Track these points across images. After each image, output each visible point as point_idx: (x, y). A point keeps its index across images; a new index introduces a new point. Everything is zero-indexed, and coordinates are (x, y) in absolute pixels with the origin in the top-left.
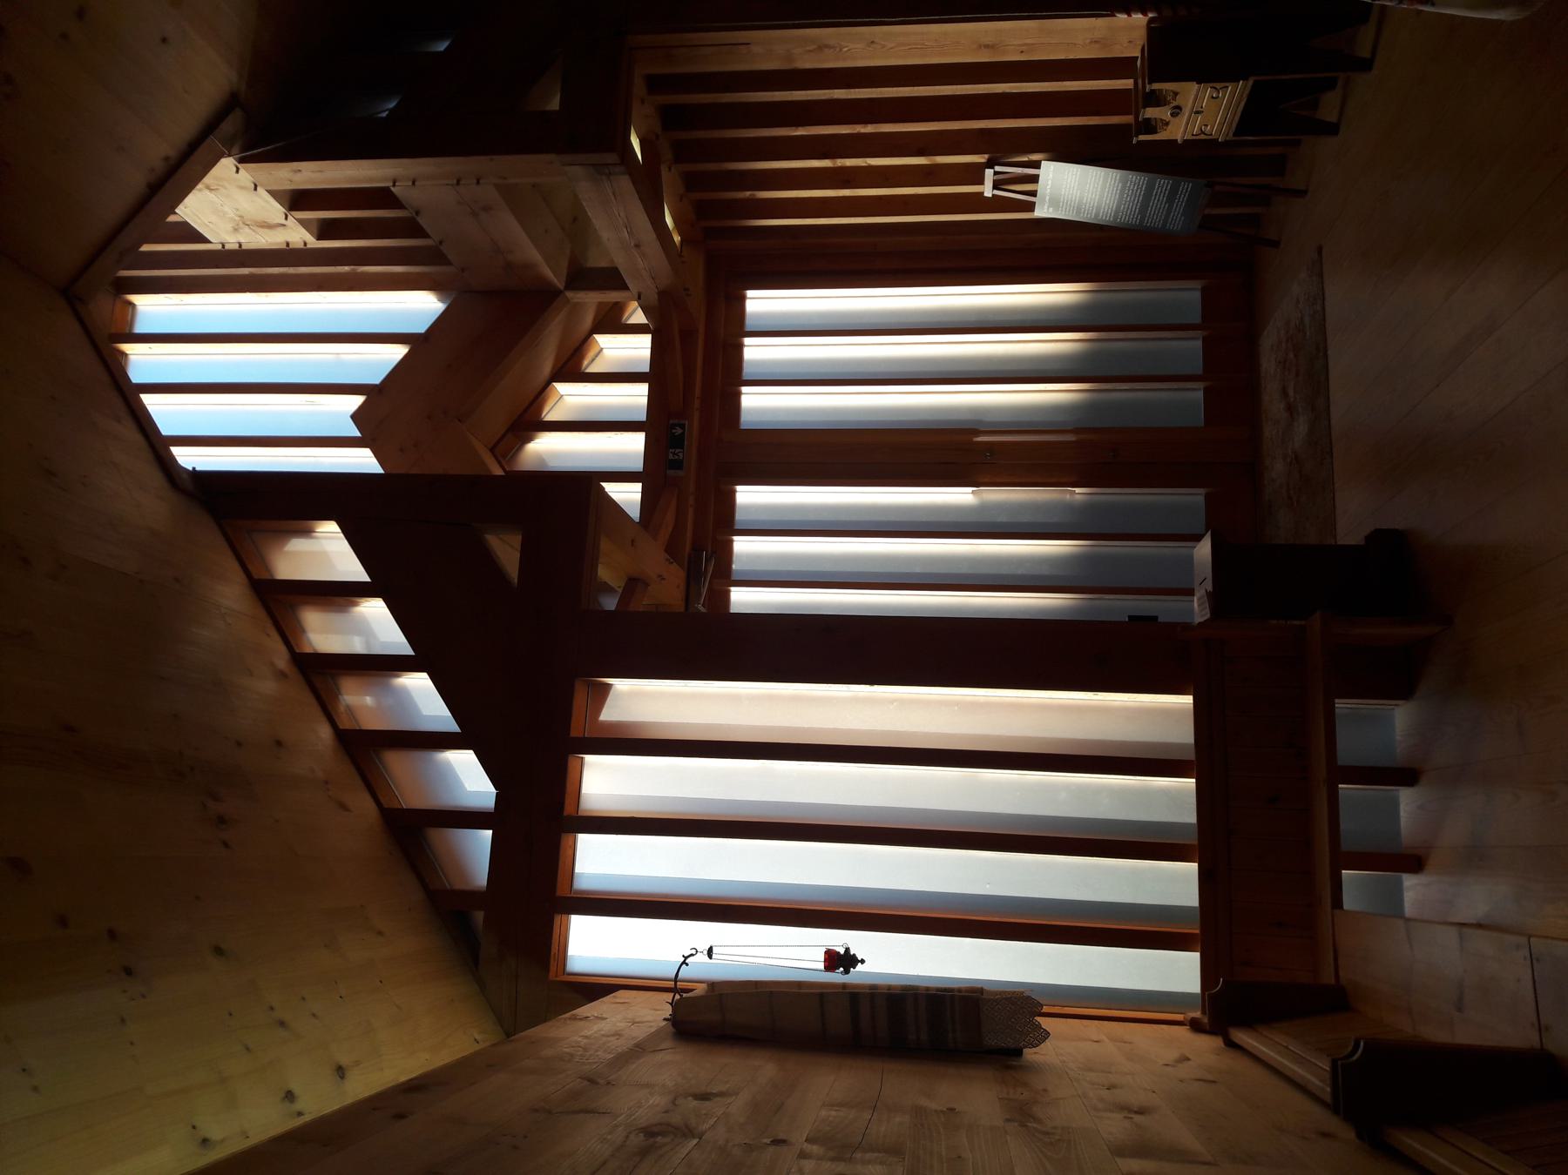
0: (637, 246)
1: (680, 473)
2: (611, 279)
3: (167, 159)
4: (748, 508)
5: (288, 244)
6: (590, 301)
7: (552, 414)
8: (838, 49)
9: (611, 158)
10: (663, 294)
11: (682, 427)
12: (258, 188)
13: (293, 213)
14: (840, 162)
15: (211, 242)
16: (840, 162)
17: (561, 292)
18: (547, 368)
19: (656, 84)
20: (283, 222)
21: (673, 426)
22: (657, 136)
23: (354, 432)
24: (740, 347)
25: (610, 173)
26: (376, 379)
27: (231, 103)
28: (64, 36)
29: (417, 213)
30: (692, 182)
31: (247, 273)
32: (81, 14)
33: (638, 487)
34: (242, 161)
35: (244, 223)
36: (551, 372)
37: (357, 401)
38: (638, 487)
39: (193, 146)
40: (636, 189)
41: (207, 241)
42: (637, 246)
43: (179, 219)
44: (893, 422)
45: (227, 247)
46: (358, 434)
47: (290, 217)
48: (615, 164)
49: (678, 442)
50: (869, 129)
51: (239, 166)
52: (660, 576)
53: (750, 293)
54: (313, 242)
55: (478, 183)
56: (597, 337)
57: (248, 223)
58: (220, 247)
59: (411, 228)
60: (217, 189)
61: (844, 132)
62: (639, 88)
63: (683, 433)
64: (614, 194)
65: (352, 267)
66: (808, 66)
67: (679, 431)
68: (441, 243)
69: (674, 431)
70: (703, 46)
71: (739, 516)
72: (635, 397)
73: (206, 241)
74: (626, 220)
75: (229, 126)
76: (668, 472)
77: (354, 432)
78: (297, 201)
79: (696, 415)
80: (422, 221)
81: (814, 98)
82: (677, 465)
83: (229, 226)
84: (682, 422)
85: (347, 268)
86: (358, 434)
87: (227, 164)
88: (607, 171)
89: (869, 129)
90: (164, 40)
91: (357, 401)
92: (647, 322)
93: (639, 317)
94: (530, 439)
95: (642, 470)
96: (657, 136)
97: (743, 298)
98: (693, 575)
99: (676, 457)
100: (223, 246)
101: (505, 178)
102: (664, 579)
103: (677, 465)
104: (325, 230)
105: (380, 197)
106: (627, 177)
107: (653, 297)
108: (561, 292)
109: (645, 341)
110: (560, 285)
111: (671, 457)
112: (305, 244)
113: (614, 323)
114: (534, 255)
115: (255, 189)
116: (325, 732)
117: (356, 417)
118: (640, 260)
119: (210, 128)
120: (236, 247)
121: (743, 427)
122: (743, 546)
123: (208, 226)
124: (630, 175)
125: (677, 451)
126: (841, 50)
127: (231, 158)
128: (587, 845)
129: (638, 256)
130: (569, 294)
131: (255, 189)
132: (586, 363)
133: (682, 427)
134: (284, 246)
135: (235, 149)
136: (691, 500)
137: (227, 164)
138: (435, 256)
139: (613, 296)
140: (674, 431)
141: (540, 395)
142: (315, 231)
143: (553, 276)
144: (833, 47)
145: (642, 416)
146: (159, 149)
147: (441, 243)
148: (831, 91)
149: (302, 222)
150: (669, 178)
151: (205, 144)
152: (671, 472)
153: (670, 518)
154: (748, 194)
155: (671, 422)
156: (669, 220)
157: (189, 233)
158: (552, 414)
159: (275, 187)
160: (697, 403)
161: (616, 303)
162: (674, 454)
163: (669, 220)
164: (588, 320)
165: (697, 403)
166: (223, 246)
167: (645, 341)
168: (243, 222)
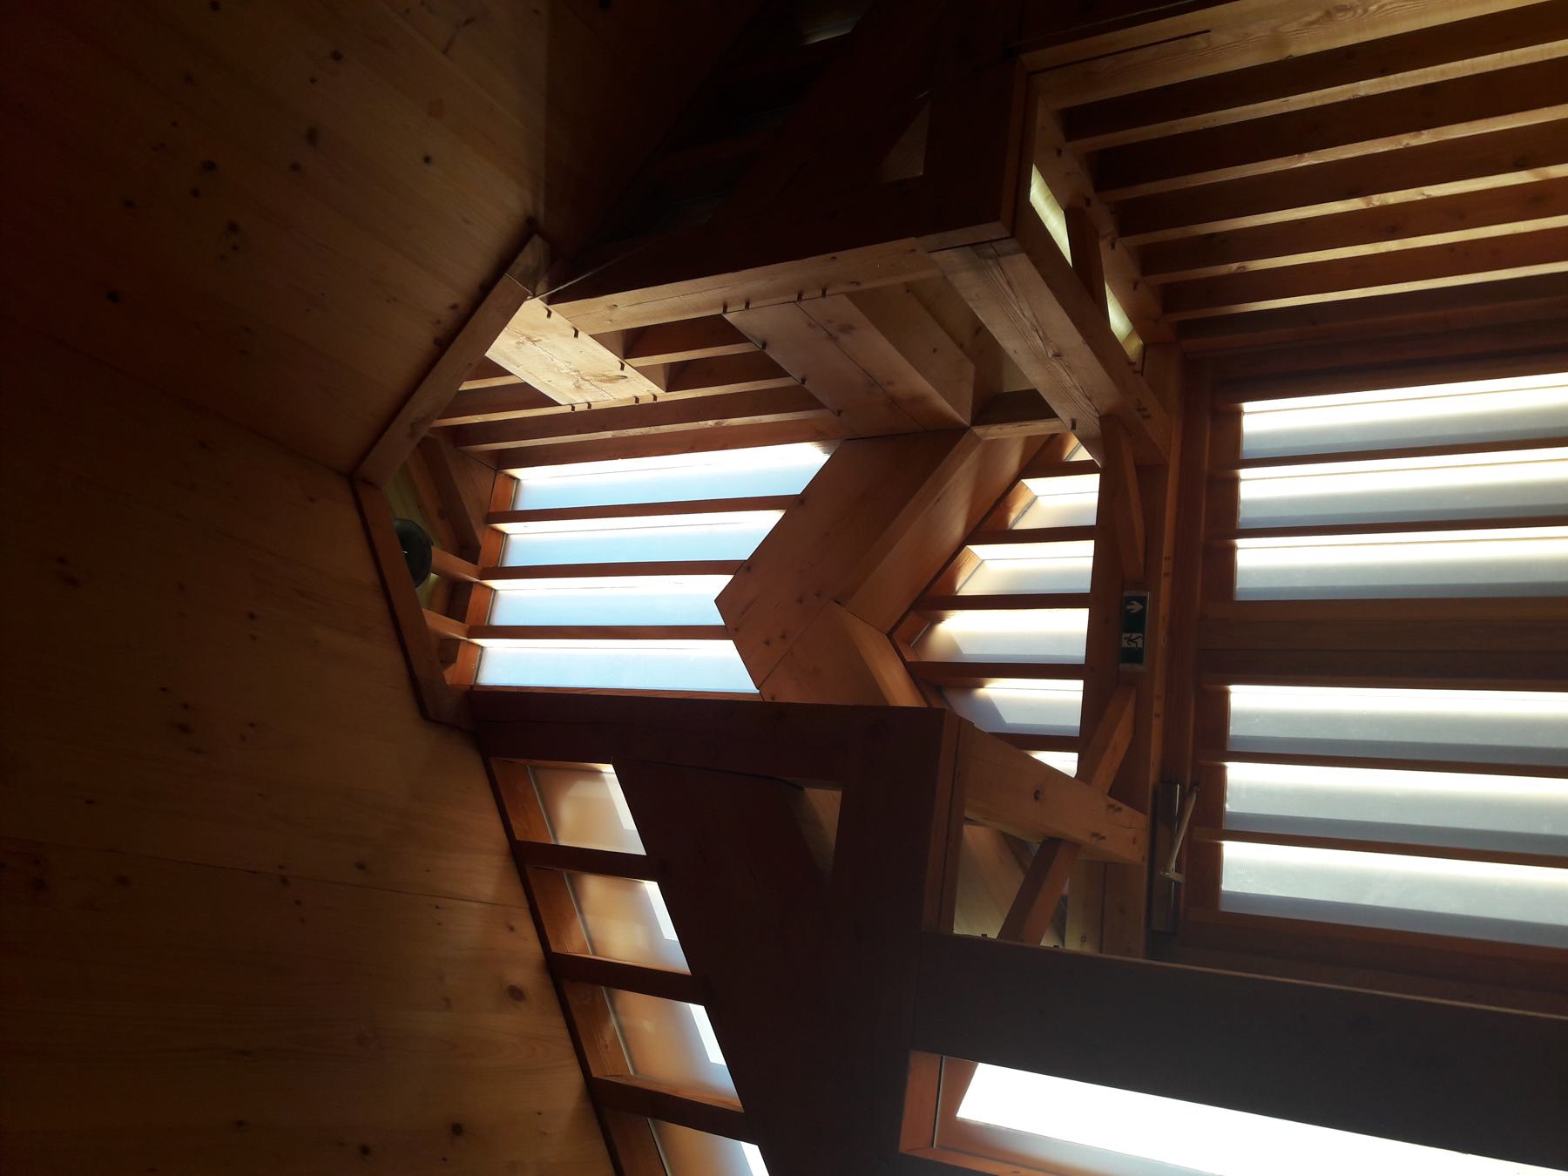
0: (1057, 355)
1: (1138, 668)
2: (1032, 406)
3: (454, 307)
4: (1249, 717)
5: (637, 400)
6: (1013, 437)
7: (969, 585)
8: (1360, 11)
9: (994, 230)
10: (1107, 419)
11: (1142, 600)
12: (580, 334)
13: (627, 360)
14: (1378, 200)
15: (560, 405)
16: (1378, 200)
17: (969, 428)
18: (958, 528)
19: (1076, 122)
20: (622, 373)
21: (1129, 600)
22: (1088, 202)
23: (718, 620)
24: (1234, 483)
25: (999, 255)
26: (744, 554)
27: (529, 228)
28: (295, 167)
29: (764, 345)
30: (1149, 261)
31: (610, 437)
32: (312, 136)
33: (1078, 685)
34: (551, 300)
35: (583, 379)
36: (965, 533)
37: (723, 581)
38: (1078, 685)
39: (486, 288)
40: (1040, 272)
41: (555, 404)
42: (1057, 355)
43: (518, 381)
44: (1459, 511)
45: (577, 409)
46: (721, 622)
47: (626, 366)
48: (1006, 238)
49: (1135, 623)
50: (1426, 138)
51: (550, 308)
52: (1095, 835)
53: (1247, 406)
54: (665, 396)
55: (824, 294)
56: (1028, 482)
57: (588, 378)
58: (569, 409)
59: (759, 365)
60: (540, 340)
61: (1381, 150)
62: (1045, 124)
63: (1143, 610)
64: (1009, 283)
65: (716, 421)
66: (1310, 49)
67: (1136, 607)
68: (803, 381)
69: (1129, 607)
70: (1135, 49)
71: (1235, 729)
72: (1077, 559)
73: (554, 404)
74: (1034, 321)
75: (529, 258)
76: (1121, 665)
77: (718, 620)
78: (632, 344)
79: (1165, 585)
80: (774, 354)
81: (1327, 101)
82: (1134, 656)
83: (570, 384)
84: (1142, 594)
85: (711, 423)
86: (721, 622)
87: (533, 308)
88: (991, 251)
89: (1426, 138)
90: (427, 160)
91: (723, 581)
92: (1091, 458)
93: (1083, 455)
94: (940, 620)
95: (1083, 663)
96: (1088, 202)
97: (1237, 415)
98: (1162, 818)
99: (1133, 645)
100: (573, 408)
101: (858, 283)
102: (1103, 838)
103: (1134, 656)
104: (675, 377)
105: (712, 329)
106: (1023, 256)
107: (1091, 423)
108: (969, 428)
109: (1092, 482)
110: (965, 420)
111: (1125, 644)
112: (655, 398)
113: (1048, 462)
114: (920, 384)
115: (576, 335)
116: (571, 1081)
117: (720, 601)
118: (1065, 374)
119: (503, 265)
120: (584, 407)
121: (1239, 598)
122: (1238, 774)
123: (548, 386)
124: (1028, 253)
125: (1134, 636)
126: (1366, 11)
127: (537, 299)
128: (1238, 774)
129: (1062, 371)
130: (979, 431)
131: (576, 335)
132: (1013, 516)
133: (1142, 600)
134: (633, 403)
135: (541, 287)
136: (1158, 707)
137: (533, 308)
138: (796, 398)
139: (1041, 428)
140: (1129, 607)
141: (949, 564)
142: (663, 381)
143: (953, 407)
144: (1352, 8)
145: (1085, 586)
146: (443, 298)
147: (803, 381)
148: (1355, 84)
149: (643, 371)
150: (1110, 256)
151: (500, 284)
152: (1125, 666)
153: (1121, 737)
154: (1234, 267)
155: (1126, 594)
156: (1118, 321)
157: (528, 395)
158: (969, 585)
159: (597, 331)
160: (1166, 566)
161: (1053, 436)
162: (1130, 640)
163: (1118, 321)
164: (1013, 462)
165: (1166, 566)
166: (573, 408)
167: (1092, 482)
168: (581, 379)
